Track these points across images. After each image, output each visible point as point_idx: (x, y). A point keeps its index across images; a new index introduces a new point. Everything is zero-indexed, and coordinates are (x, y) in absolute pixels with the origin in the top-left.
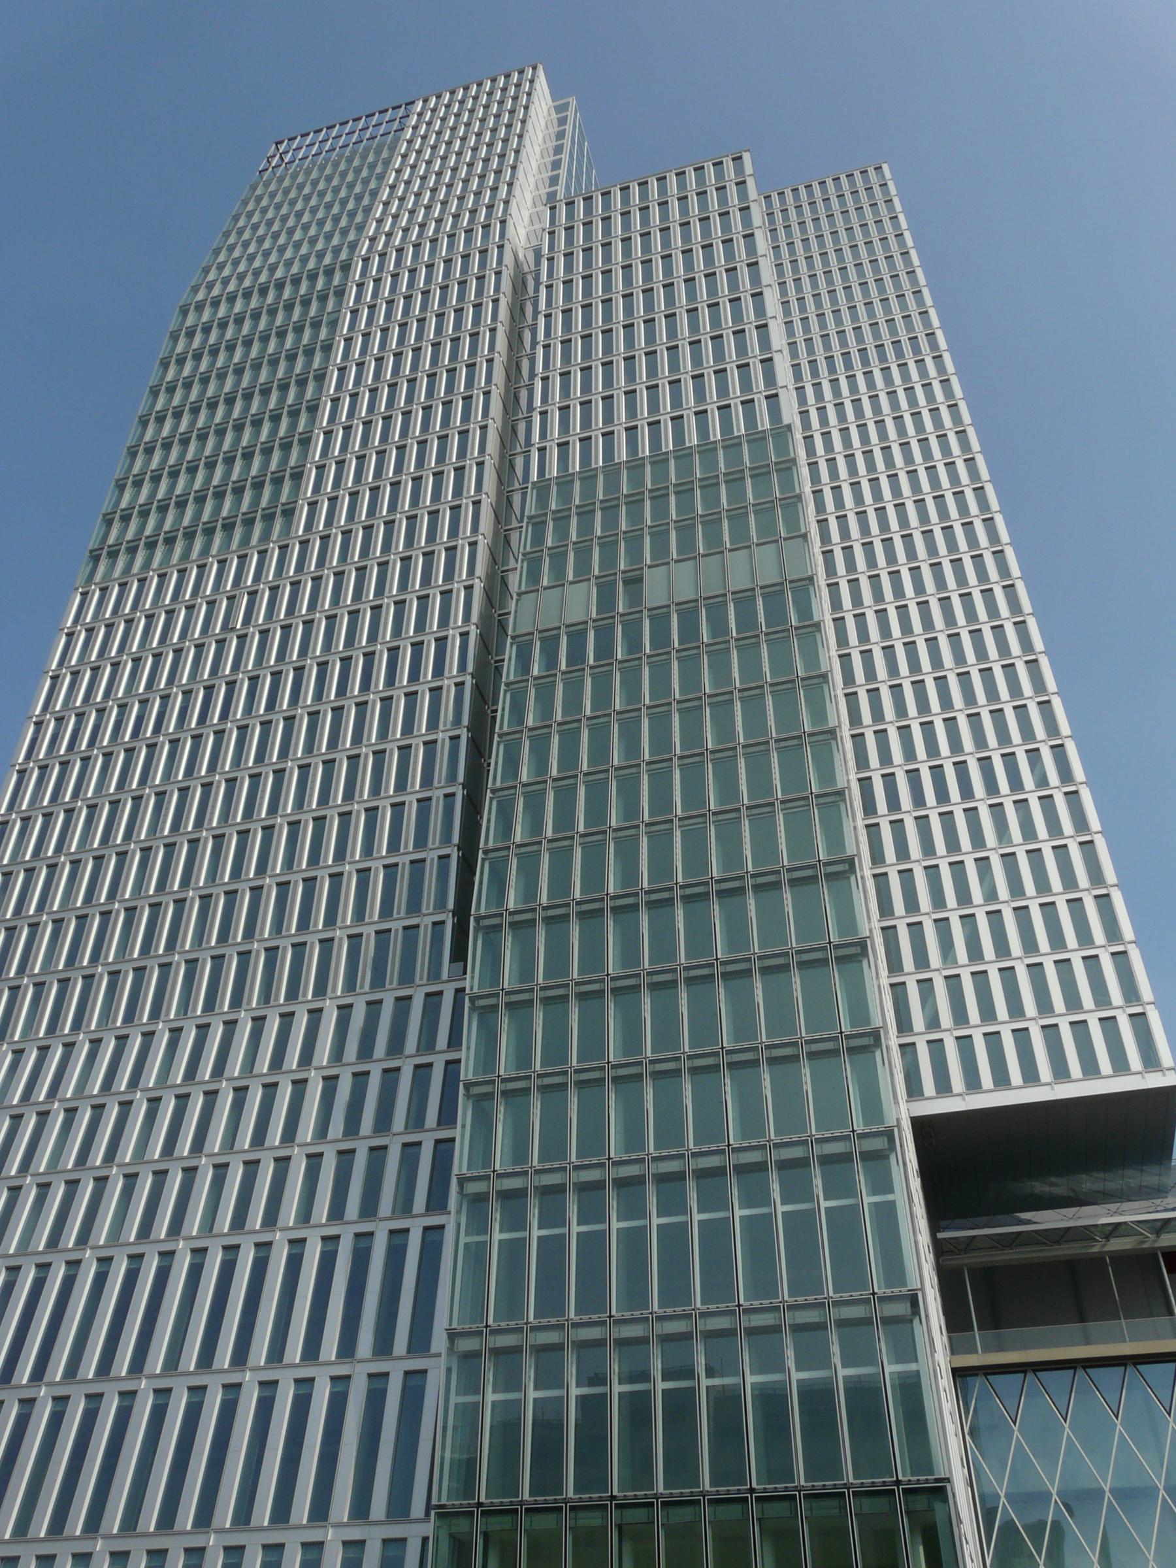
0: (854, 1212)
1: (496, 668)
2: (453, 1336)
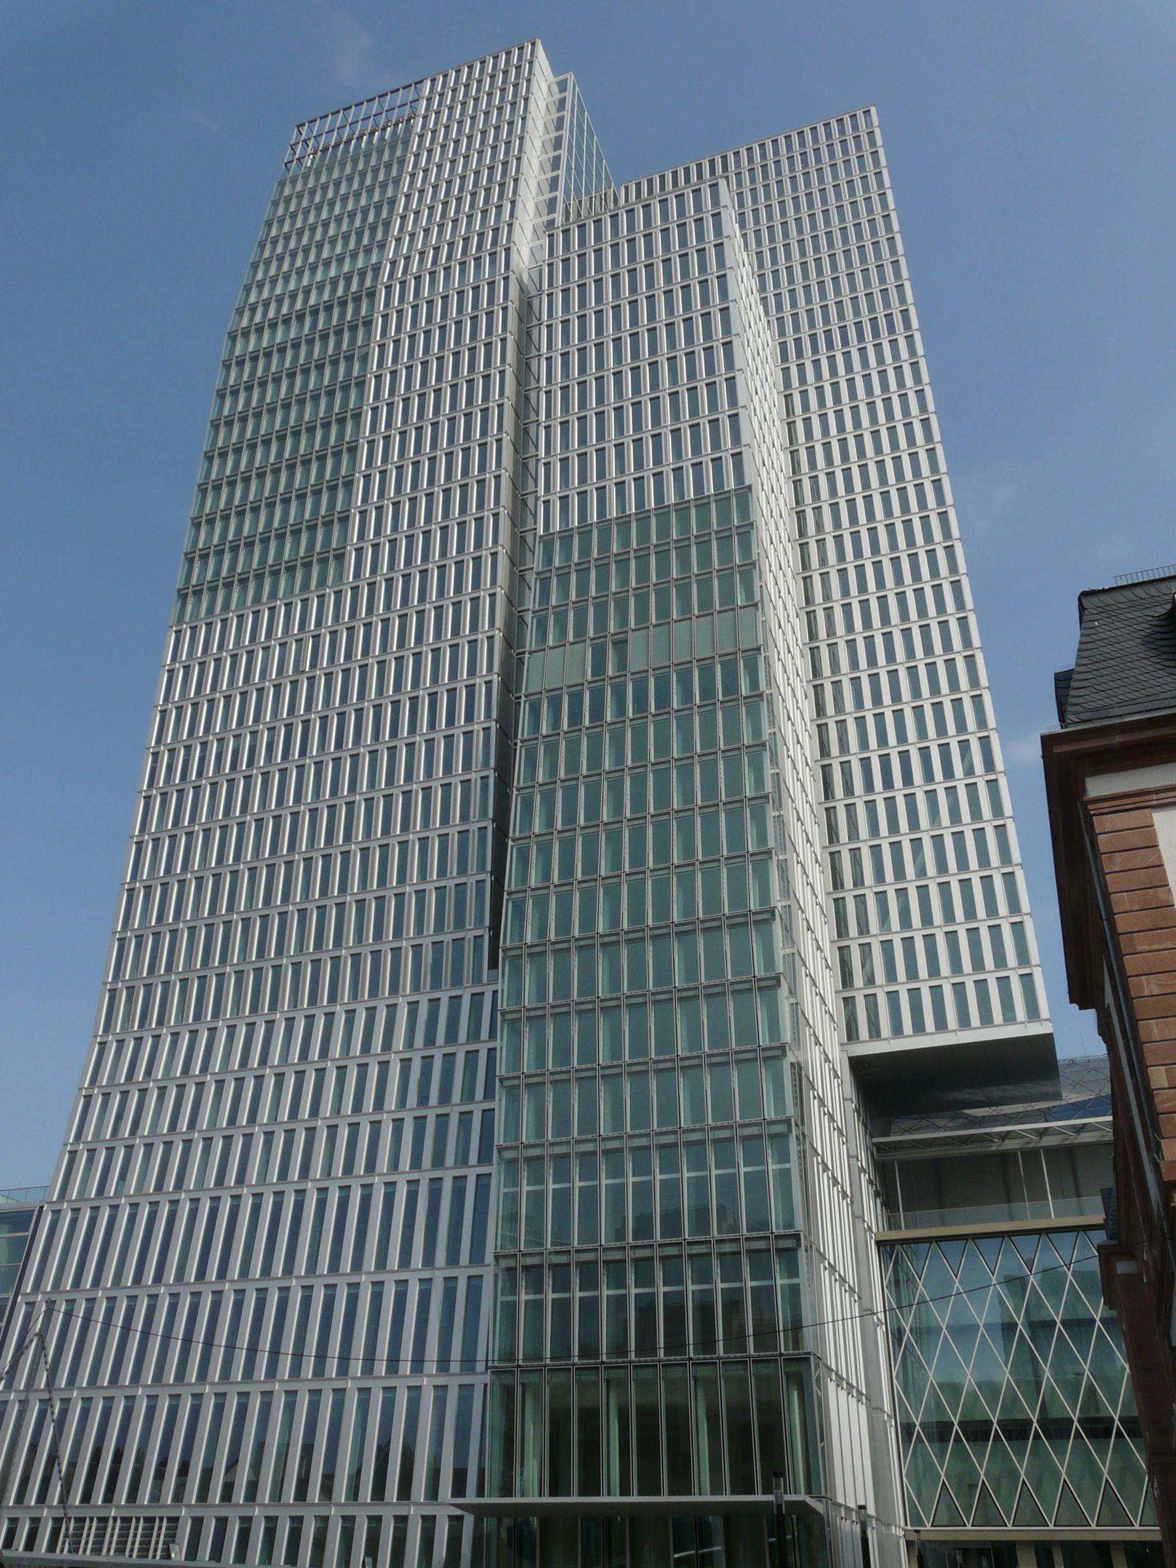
0: (770, 1291)
1: (521, 576)
2: (497, 1258)
